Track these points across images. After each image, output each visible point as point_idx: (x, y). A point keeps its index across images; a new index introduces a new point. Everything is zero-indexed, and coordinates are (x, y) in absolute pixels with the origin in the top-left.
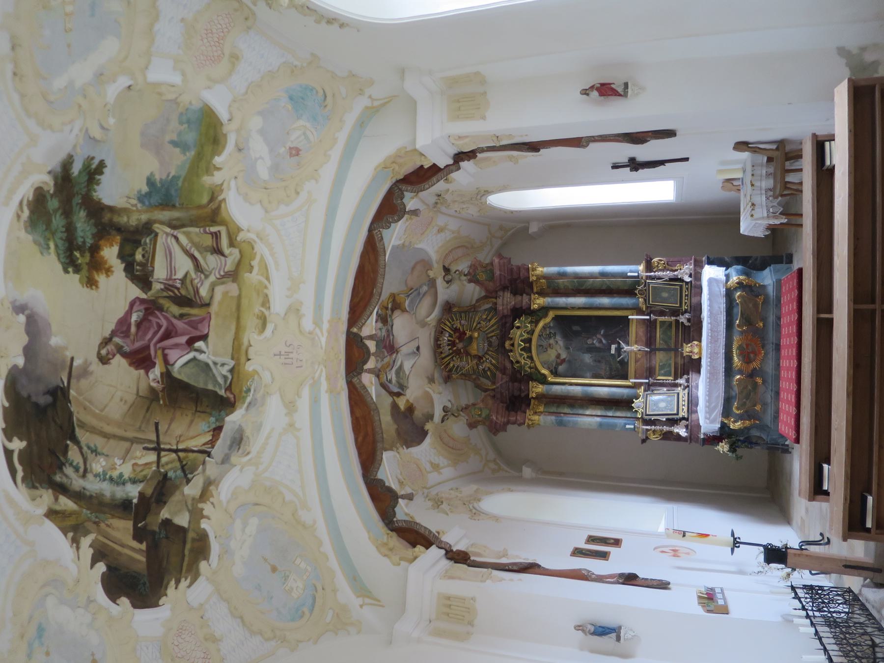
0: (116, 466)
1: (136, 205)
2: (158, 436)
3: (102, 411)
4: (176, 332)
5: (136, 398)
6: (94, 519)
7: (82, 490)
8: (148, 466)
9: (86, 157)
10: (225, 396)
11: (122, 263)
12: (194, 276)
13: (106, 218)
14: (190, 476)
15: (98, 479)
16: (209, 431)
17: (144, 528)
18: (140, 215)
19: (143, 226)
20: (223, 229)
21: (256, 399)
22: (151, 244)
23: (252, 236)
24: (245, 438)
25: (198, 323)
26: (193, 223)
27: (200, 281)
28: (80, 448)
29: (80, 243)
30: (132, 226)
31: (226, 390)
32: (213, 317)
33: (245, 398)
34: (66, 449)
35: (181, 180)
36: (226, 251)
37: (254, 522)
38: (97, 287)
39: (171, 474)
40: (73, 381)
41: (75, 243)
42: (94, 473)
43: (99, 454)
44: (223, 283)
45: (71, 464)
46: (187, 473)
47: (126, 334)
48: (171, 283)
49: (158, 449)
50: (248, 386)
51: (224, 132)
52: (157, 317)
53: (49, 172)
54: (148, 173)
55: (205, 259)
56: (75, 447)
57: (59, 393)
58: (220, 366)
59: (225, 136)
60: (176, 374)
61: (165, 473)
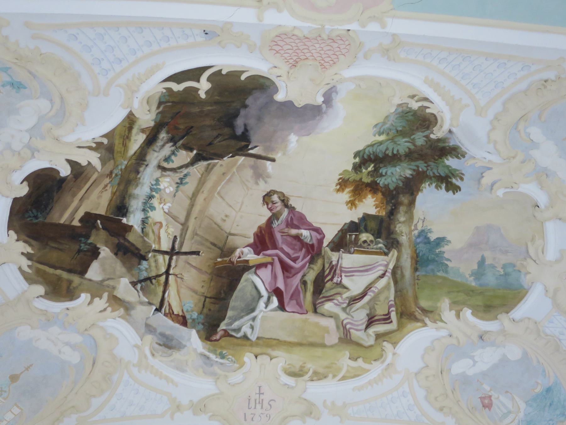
0: (163, 204)
1: (417, 229)
2: (186, 253)
3: (219, 193)
4: (288, 277)
5: (226, 233)
6: (115, 172)
7: (146, 163)
8: (157, 239)
9: (463, 172)
10: (219, 329)
11: (358, 219)
12: (345, 296)
13: (403, 199)
14: (139, 286)
15: (154, 183)
16: (182, 311)
17: (95, 226)
18: (406, 234)
19: (395, 239)
20: (393, 326)
21: (212, 365)
22: (377, 249)
23: (389, 359)
24: (170, 351)
25: (297, 300)
26: (400, 293)
27: (339, 302)
28: (186, 166)
29: (380, 171)
30: (395, 227)
31: (225, 331)
32: (304, 316)
33: (214, 352)
34: (189, 149)
35: (444, 275)
36: (372, 331)
37: (74, 358)
38: (338, 191)
39: (145, 264)
40: (252, 160)
41: (381, 165)
42: (160, 179)
43: (178, 187)
44: (338, 327)
45: (173, 153)
46: (143, 283)
47: (290, 224)
48: (338, 272)
49: (172, 253)
50: (227, 355)
51: (499, 316)
52: (304, 257)
53: (450, 131)
54: (449, 238)
55: (363, 307)
56: (189, 160)
57: (243, 143)
58: (251, 325)
59: (496, 318)
60: (246, 276)
61: (147, 259)
